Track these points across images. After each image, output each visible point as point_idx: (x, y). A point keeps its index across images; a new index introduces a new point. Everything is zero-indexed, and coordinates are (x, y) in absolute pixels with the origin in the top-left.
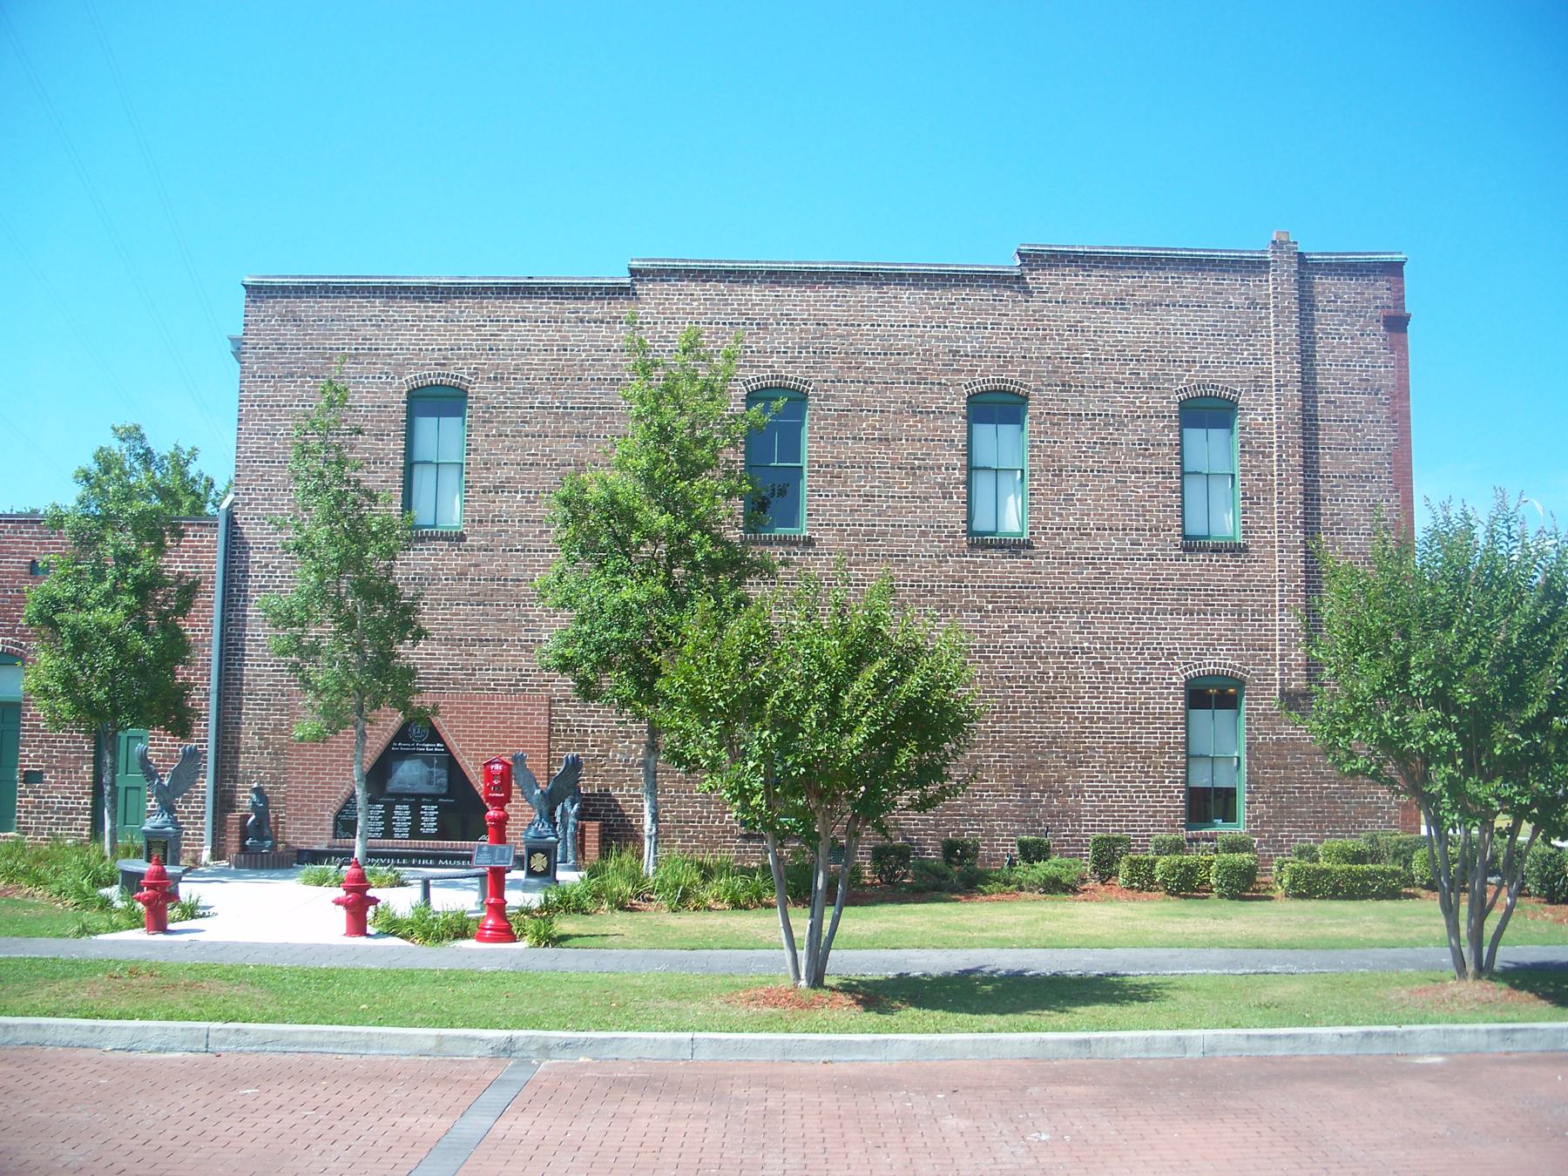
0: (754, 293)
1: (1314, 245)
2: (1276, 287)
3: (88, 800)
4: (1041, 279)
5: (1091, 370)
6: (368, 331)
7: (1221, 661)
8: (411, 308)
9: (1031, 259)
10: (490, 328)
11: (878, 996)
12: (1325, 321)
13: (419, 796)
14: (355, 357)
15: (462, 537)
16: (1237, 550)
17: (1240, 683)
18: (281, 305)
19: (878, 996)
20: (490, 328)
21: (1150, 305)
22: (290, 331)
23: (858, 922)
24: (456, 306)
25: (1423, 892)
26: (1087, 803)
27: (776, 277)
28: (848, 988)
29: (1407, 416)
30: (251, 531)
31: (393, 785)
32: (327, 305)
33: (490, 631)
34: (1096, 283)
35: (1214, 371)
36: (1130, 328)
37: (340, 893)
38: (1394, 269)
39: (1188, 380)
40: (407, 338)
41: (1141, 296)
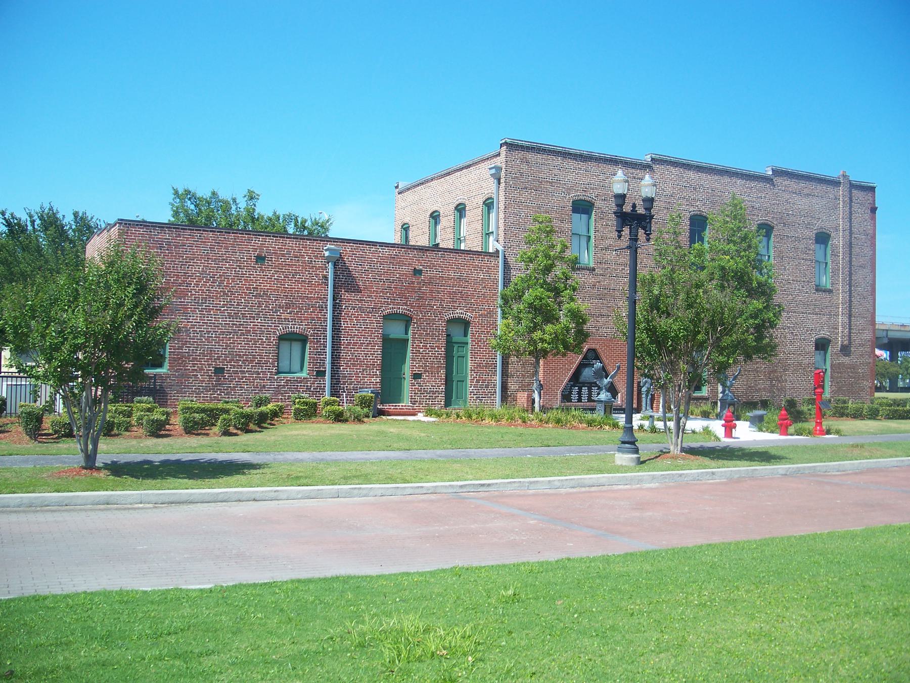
0: (691, 174)
1: (854, 177)
2: (841, 191)
3: (443, 387)
4: (778, 180)
5: (792, 219)
6: (556, 172)
7: (824, 333)
8: (571, 164)
9: (777, 172)
10: (602, 177)
11: (118, 470)
12: (855, 207)
13: (591, 383)
14: (551, 183)
15: (594, 269)
16: (830, 291)
17: (830, 341)
18: (520, 154)
19: (118, 470)
20: (602, 177)
21: (808, 195)
22: (525, 167)
23: (104, 445)
24: (591, 165)
25: (239, 432)
26: (788, 385)
27: (699, 168)
28: (107, 466)
29: (875, 245)
30: (512, 260)
31: (582, 379)
32: (539, 157)
33: (604, 312)
34: (793, 184)
35: (824, 223)
36: (802, 203)
37: (723, 422)
38: (872, 189)
39: (818, 225)
40: (571, 176)
41: (806, 191)
